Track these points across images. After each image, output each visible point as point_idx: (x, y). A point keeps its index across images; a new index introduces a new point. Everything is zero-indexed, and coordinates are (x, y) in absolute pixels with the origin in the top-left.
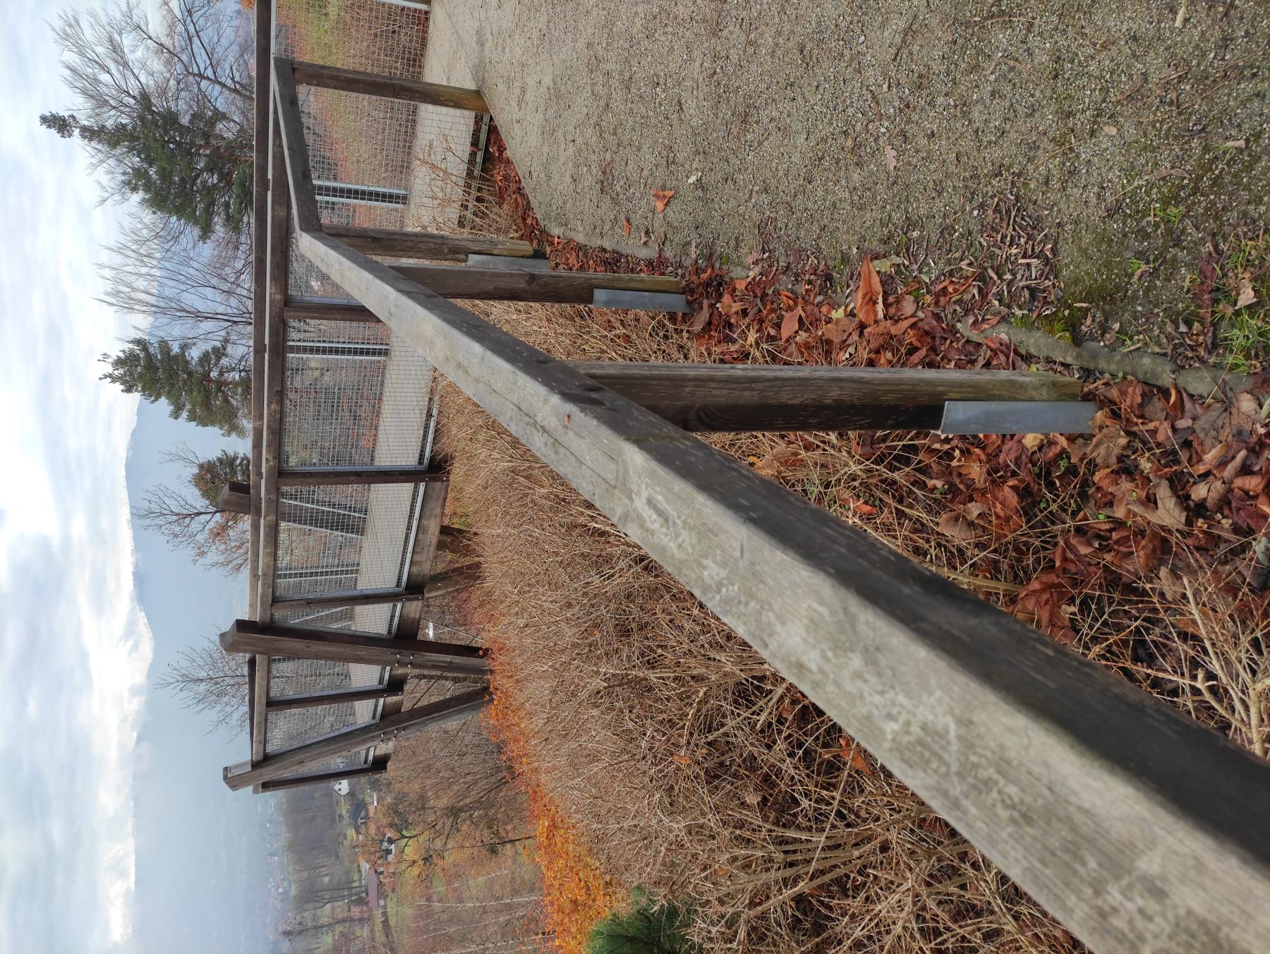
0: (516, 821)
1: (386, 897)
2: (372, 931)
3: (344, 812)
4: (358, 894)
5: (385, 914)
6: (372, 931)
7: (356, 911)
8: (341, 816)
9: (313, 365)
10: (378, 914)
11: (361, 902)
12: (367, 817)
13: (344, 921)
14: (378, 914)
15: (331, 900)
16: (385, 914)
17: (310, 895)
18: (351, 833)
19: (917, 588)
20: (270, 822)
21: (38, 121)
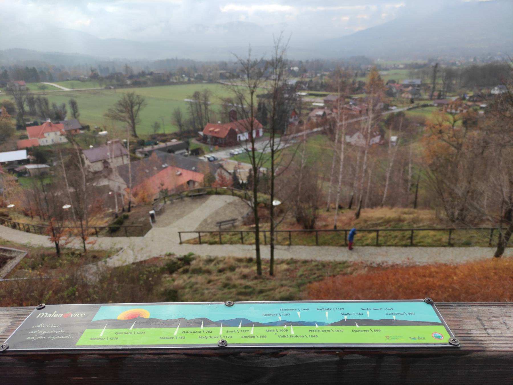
0: (302, 211)
1: (437, 106)
2: (426, 100)
3: (483, 91)
4: (443, 95)
5: (431, 106)
6: (426, 100)
7: (436, 93)
8: (481, 89)
9: (285, 226)
10: (432, 103)
11: (439, 97)
12: (476, 101)
13: (434, 88)
14: (432, 103)
15: (444, 84)
16: (431, 106)
17: (450, 74)
18: (471, 94)
19: (171, 288)
20: (490, 58)
21: (179, 245)
